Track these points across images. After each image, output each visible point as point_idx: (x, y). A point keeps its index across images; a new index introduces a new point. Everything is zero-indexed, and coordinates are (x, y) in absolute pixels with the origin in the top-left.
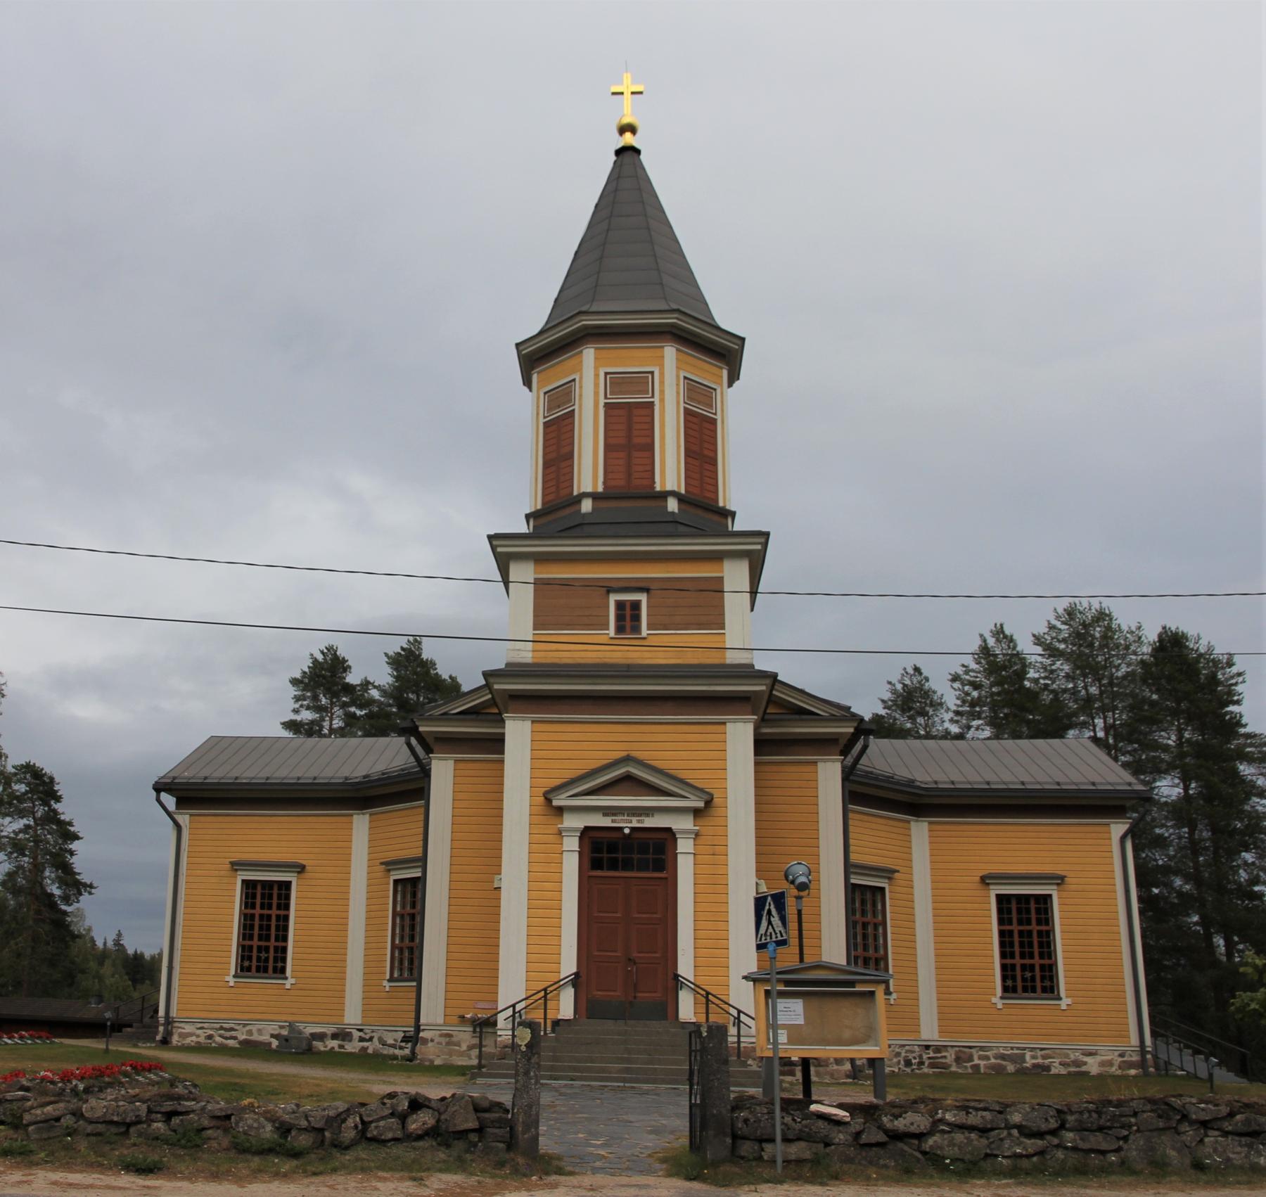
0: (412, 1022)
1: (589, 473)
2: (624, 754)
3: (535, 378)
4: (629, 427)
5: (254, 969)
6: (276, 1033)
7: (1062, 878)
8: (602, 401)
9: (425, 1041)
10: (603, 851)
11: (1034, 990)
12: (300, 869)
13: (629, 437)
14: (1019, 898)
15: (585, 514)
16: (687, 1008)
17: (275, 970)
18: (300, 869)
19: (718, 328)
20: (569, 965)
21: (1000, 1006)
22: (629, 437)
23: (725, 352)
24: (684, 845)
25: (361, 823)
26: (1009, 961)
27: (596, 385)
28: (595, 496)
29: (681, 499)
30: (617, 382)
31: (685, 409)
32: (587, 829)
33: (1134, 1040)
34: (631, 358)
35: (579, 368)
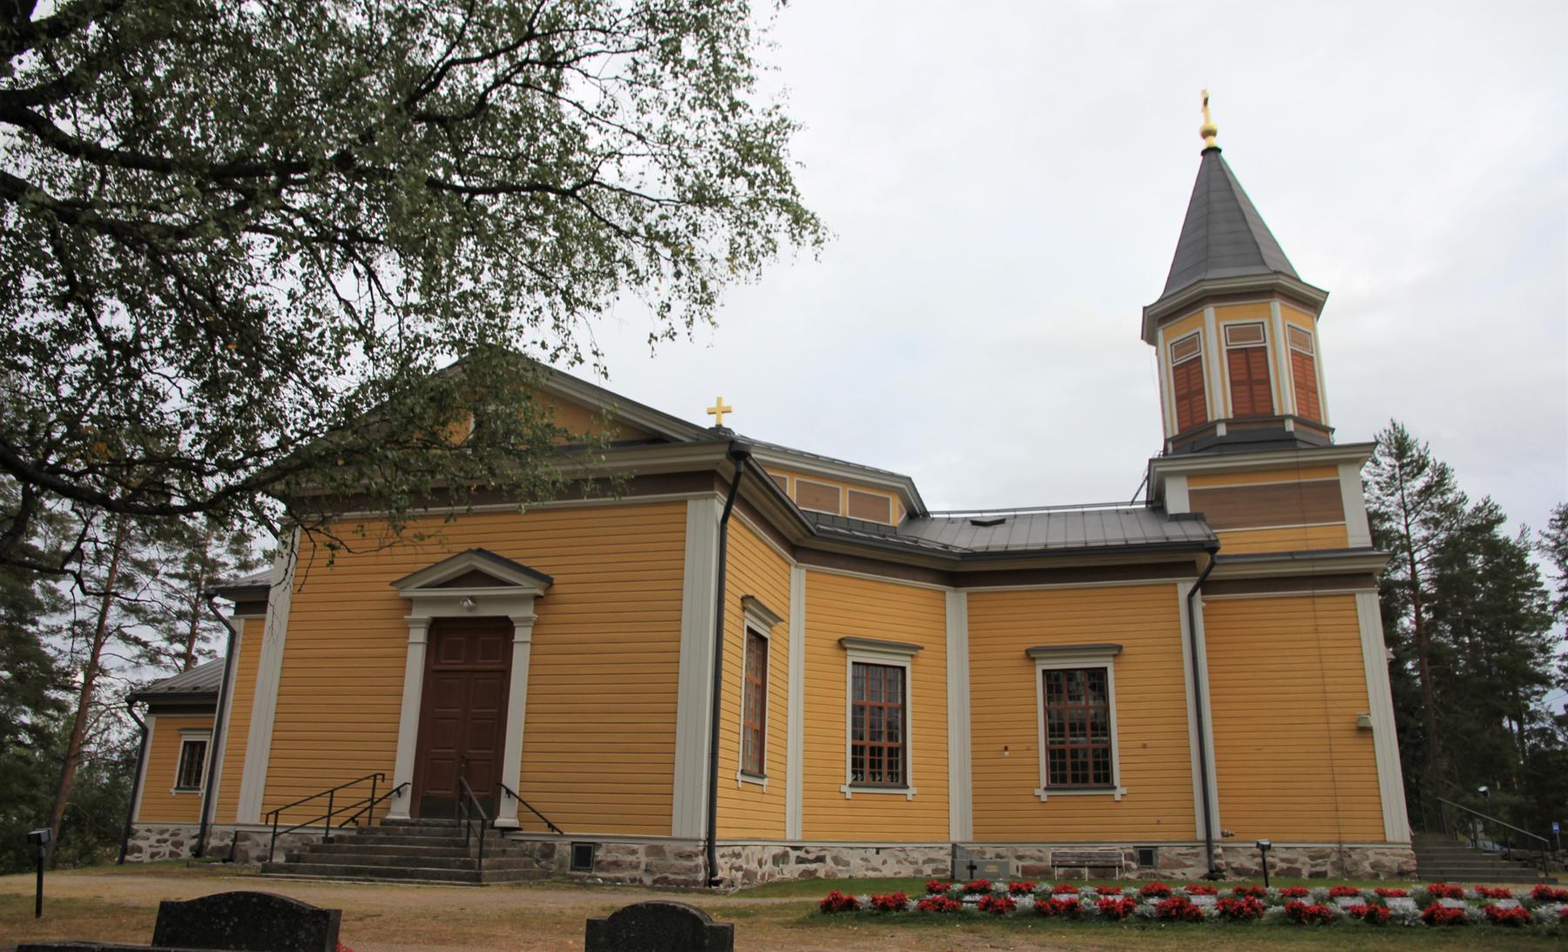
1: (1219, 403)
3: (1160, 334)
4: (1249, 367)
7: (1120, 648)
8: (1224, 349)
11: (1085, 779)
13: (1249, 375)
19: (1298, 280)
21: (1044, 798)
22: (1249, 375)
23: (1311, 302)
24: (522, 635)
26: (859, 743)
27: (1218, 334)
28: (1228, 422)
29: (1297, 420)
30: (1235, 333)
31: (1294, 353)
34: (1243, 314)
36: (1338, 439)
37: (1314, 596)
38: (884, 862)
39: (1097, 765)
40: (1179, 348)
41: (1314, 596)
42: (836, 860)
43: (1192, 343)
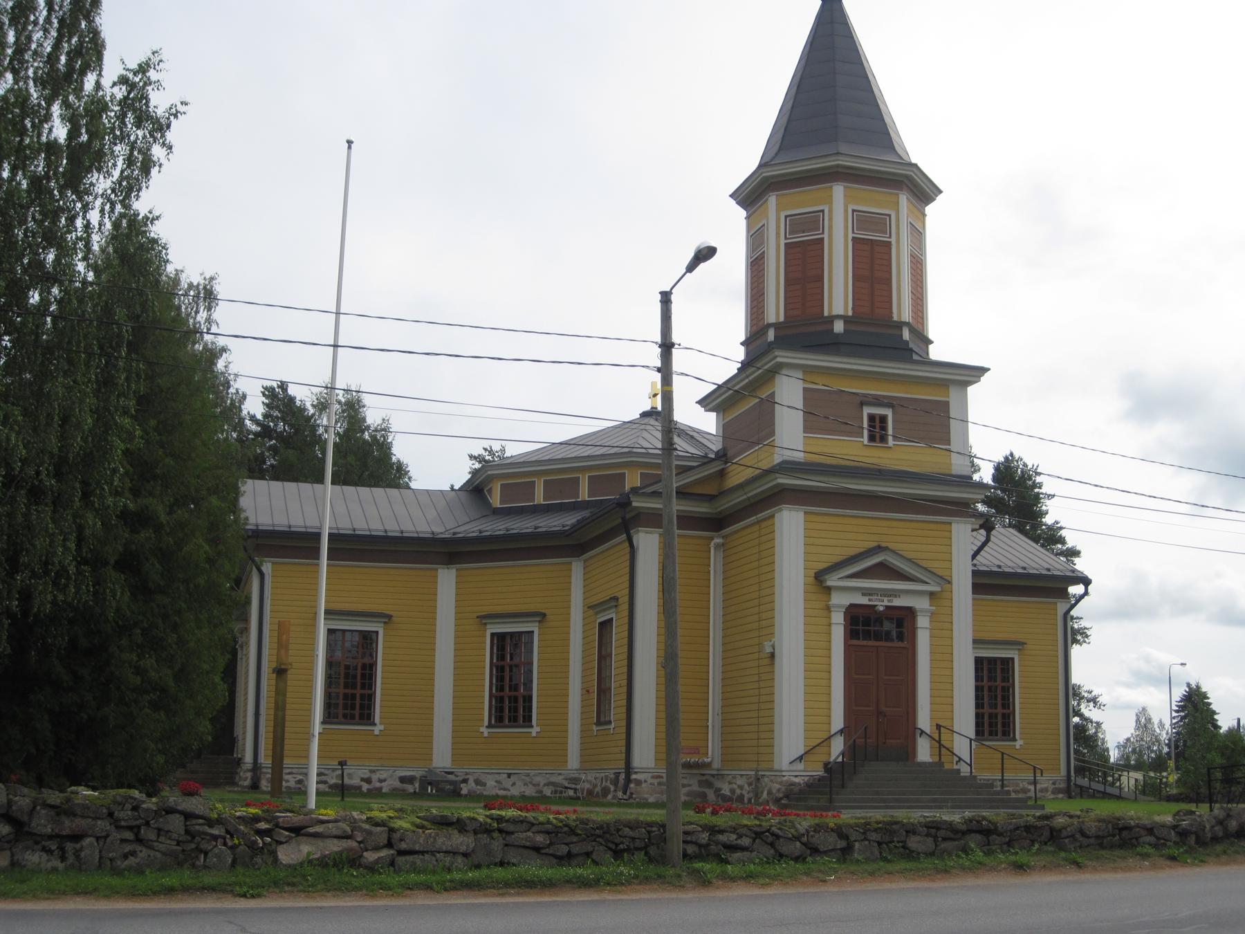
0: (622, 764)
1: (839, 298)
2: (875, 544)
5: (340, 715)
6: (366, 776)
9: (638, 783)
10: (863, 624)
12: (387, 618)
14: (512, 634)
15: (838, 335)
16: (924, 752)
17: (362, 717)
18: (387, 618)
20: (838, 722)
23: (922, 191)
24: (923, 622)
25: (447, 579)
28: (846, 320)
30: (862, 220)
32: (851, 605)
33: (1063, 772)
35: (829, 200)
36: (935, 353)
37: (759, 522)
38: (514, 784)
39: (363, 676)
40: (797, 223)
41: (759, 522)
42: (477, 782)
43: (813, 221)
